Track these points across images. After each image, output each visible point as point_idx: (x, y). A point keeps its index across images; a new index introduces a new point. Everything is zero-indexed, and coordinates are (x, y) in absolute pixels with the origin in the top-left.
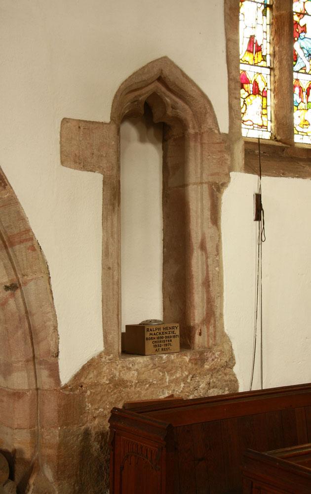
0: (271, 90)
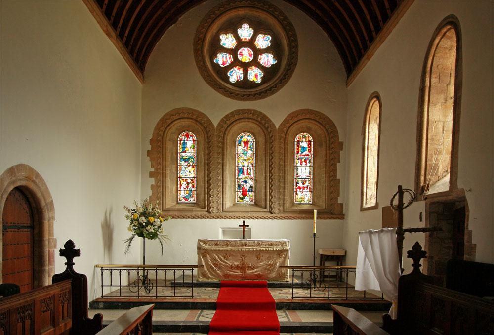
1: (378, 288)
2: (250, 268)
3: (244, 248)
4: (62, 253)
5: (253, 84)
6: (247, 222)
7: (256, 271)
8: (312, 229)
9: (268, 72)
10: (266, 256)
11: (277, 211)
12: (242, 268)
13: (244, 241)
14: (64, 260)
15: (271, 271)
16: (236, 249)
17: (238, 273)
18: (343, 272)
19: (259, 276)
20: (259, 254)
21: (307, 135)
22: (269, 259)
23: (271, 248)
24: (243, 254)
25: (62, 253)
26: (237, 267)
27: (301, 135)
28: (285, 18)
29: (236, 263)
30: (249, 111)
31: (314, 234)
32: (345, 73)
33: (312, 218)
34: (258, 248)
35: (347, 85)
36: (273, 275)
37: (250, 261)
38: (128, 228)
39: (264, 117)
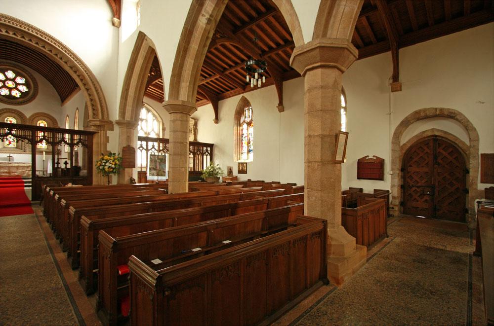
1: (66, 146)
2: (13, 173)
3: (10, 165)
4: (64, 163)
5: (14, 98)
6: (11, 155)
7: (17, 174)
8: (43, 157)
9: (24, 94)
10: (21, 168)
11: (28, 151)
12: (9, 173)
13: (10, 162)
14: (65, 165)
15: (24, 173)
16: (6, 165)
17: (7, 174)
18: (207, 8)
19: (18, 176)
20: (18, 167)
21: (44, 122)
22: (23, 169)
23: (24, 165)
24: (9, 167)
25: (64, 163)
26: (6, 172)
27: (41, 121)
28: (32, 76)
29: (6, 171)
30: (12, 110)
31: (44, 161)
32: (61, 102)
33: (43, 154)
34: (16, 165)
35: (62, 106)
36: (25, 175)
37: (12, 170)
38: (250, 180)
39: (21, 113)
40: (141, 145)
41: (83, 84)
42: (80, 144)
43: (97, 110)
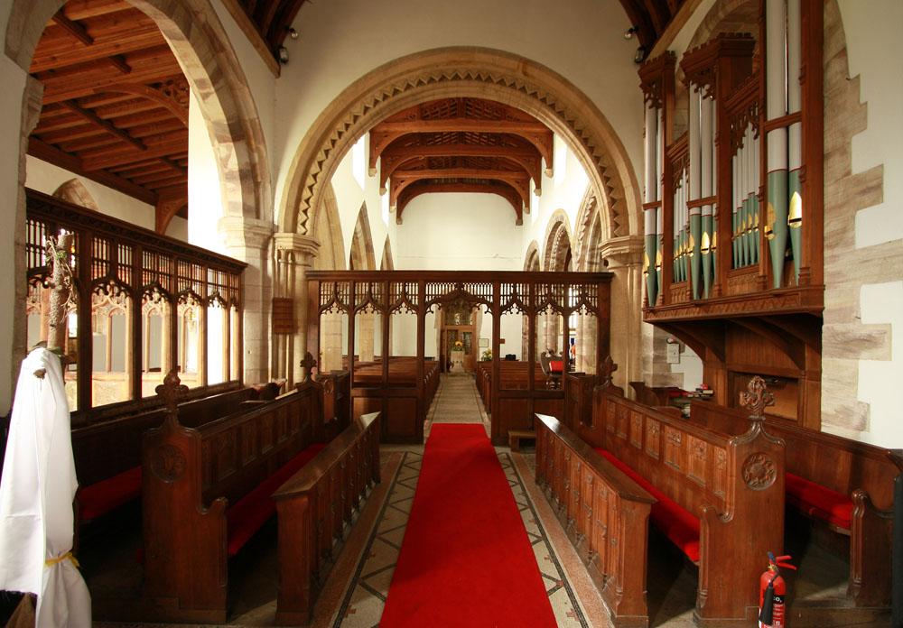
0: (346, 295)
40: (405, 294)
41: (550, 106)
42: (515, 305)
43: (623, 201)
